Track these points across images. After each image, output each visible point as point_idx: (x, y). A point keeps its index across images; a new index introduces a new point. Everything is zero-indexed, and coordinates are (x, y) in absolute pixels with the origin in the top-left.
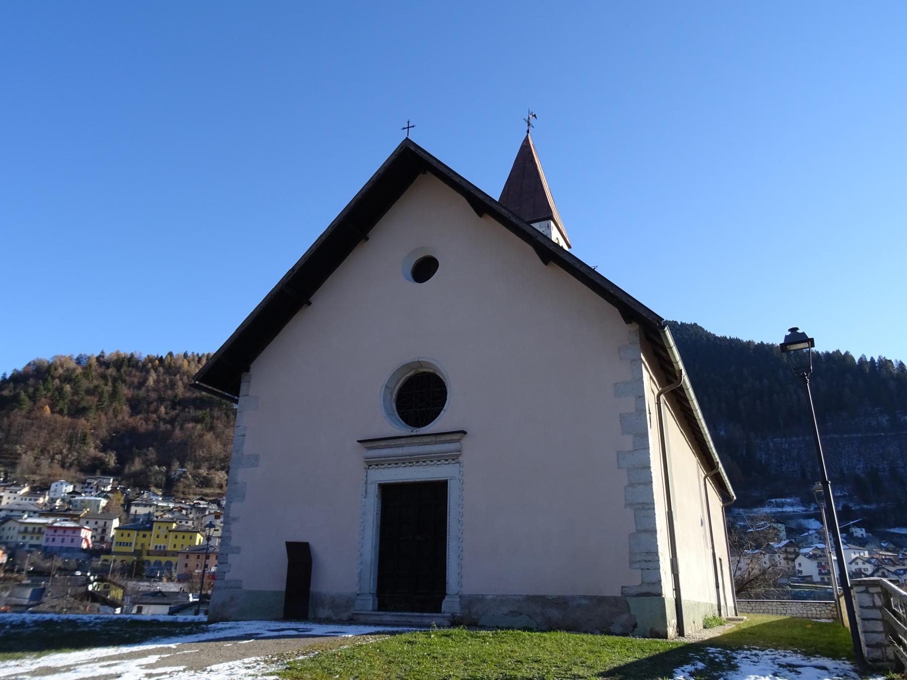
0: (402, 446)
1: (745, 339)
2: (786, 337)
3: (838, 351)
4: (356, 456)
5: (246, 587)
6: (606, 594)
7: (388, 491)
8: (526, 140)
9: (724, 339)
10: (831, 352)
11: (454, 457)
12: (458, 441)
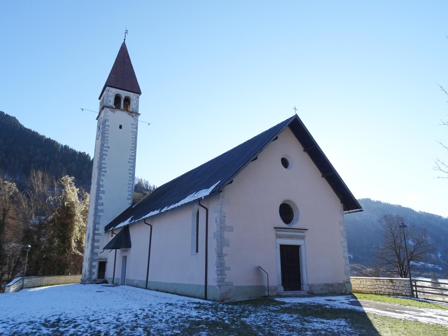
0: (290, 231)
1: (41, 133)
2: (31, 130)
3: (85, 153)
4: (273, 233)
5: (235, 284)
6: (341, 282)
7: (282, 247)
8: (124, 44)
9: (29, 130)
10: (81, 152)
11: (303, 238)
12: (303, 232)
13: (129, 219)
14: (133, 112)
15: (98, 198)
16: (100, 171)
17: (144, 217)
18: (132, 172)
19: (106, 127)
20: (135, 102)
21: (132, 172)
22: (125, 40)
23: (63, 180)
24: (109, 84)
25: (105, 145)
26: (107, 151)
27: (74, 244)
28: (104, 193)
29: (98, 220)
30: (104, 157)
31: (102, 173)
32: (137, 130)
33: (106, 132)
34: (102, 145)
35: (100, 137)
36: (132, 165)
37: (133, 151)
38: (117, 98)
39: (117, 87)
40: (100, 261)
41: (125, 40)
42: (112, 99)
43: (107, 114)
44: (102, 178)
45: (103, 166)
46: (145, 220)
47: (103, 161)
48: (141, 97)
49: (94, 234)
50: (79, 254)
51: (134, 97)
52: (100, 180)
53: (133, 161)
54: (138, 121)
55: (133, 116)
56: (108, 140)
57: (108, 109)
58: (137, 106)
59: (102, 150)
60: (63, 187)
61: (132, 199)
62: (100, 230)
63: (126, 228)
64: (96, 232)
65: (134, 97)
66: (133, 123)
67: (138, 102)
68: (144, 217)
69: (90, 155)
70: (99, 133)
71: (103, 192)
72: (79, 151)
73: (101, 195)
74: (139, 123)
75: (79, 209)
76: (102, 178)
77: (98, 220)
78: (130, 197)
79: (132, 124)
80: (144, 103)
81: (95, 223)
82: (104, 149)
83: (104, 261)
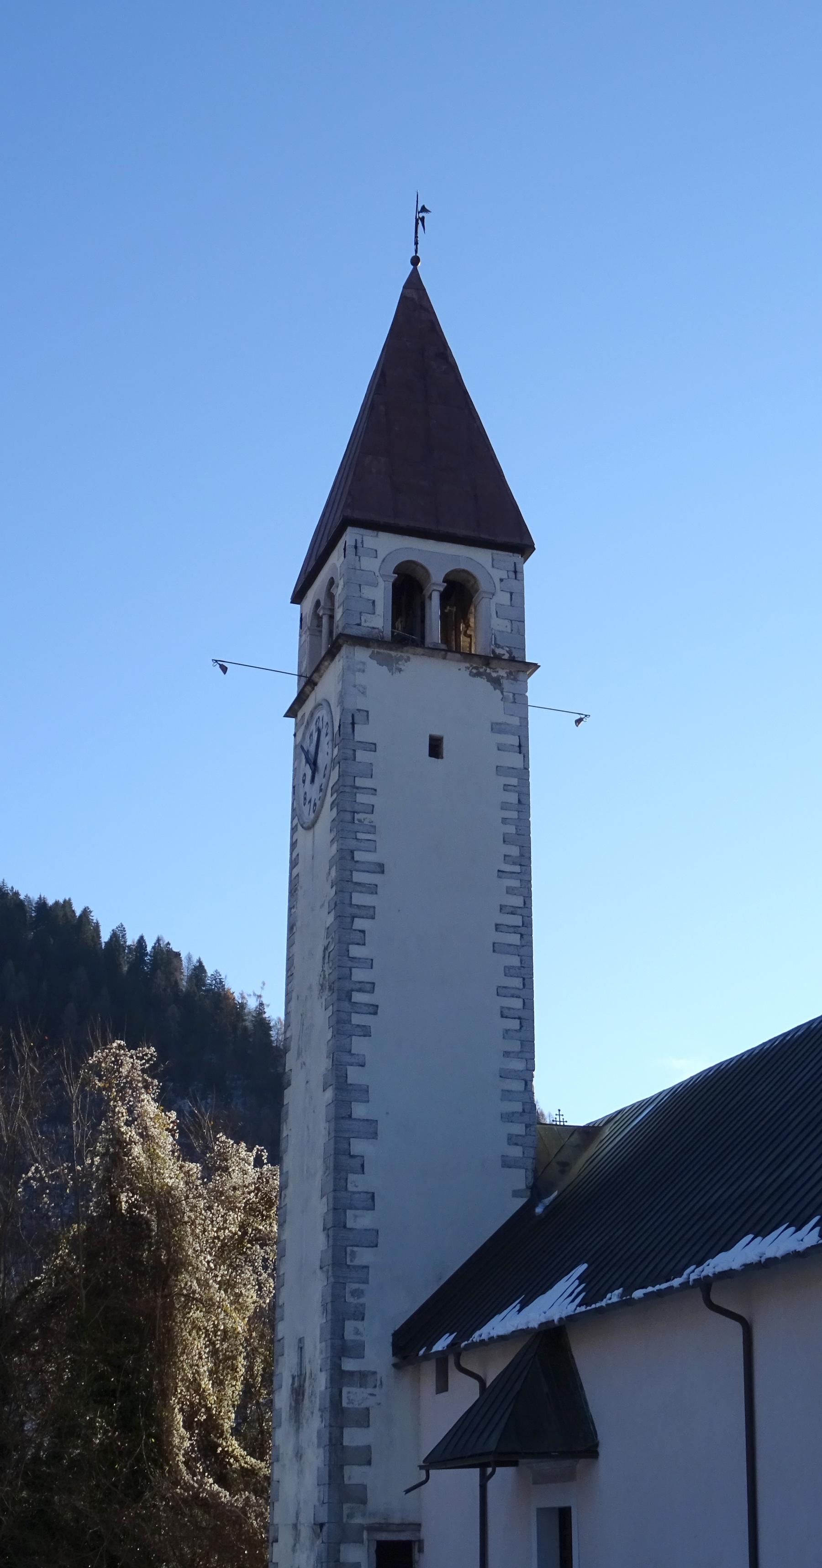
3: (68, 904)
8: (414, 284)
13: (568, 1284)
14: (498, 657)
15: (342, 1163)
16: (346, 1005)
17: (693, 1274)
18: (517, 1003)
19: (361, 755)
20: (503, 598)
21: (517, 1003)
22: (415, 261)
23: (96, 1069)
24: (357, 515)
25: (358, 856)
26: (373, 889)
27: (182, 1440)
28: (374, 1135)
29: (354, 1293)
30: (359, 924)
31: (356, 1019)
32: (526, 757)
33: (359, 782)
34: (345, 860)
35: (327, 815)
36: (515, 961)
37: (515, 883)
38: (407, 585)
39: (402, 523)
40: (384, 1536)
41: (415, 261)
42: (381, 594)
43: (360, 679)
44: (359, 1045)
45: (359, 975)
46: (705, 1285)
47: (356, 951)
48: (531, 567)
49: (339, 1378)
50: (215, 1495)
51: (497, 574)
52: (346, 1058)
53: (515, 939)
54: (525, 705)
55: (496, 683)
56: (372, 829)
57: (362, 654)
58: (518, 622)
59: (344, 885)
60: (99, 1109)
61: (529, 1163)
62: (368, 1351)
63: (552, 1339)
64: (349, 1365)
65: (497, 574)
66: (502, 718)
67: (517, 597)
68: (693, 1274)
69: (95, 916)
70: (313, 792)
71: (371, 1130)
72: (35, 897)
73: (358, 1147)
74: (534, 717)
75: (203, 1232)
76: (359, 1045)
77: (354, 1293)
78: (516, 1152)
79: (497, 728)
80: (559, 605)
81: (340, 1312)
82: (358, 877)
83: (404, 1537)
